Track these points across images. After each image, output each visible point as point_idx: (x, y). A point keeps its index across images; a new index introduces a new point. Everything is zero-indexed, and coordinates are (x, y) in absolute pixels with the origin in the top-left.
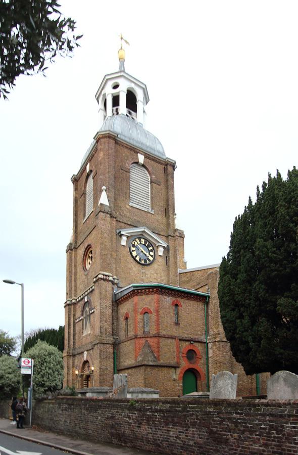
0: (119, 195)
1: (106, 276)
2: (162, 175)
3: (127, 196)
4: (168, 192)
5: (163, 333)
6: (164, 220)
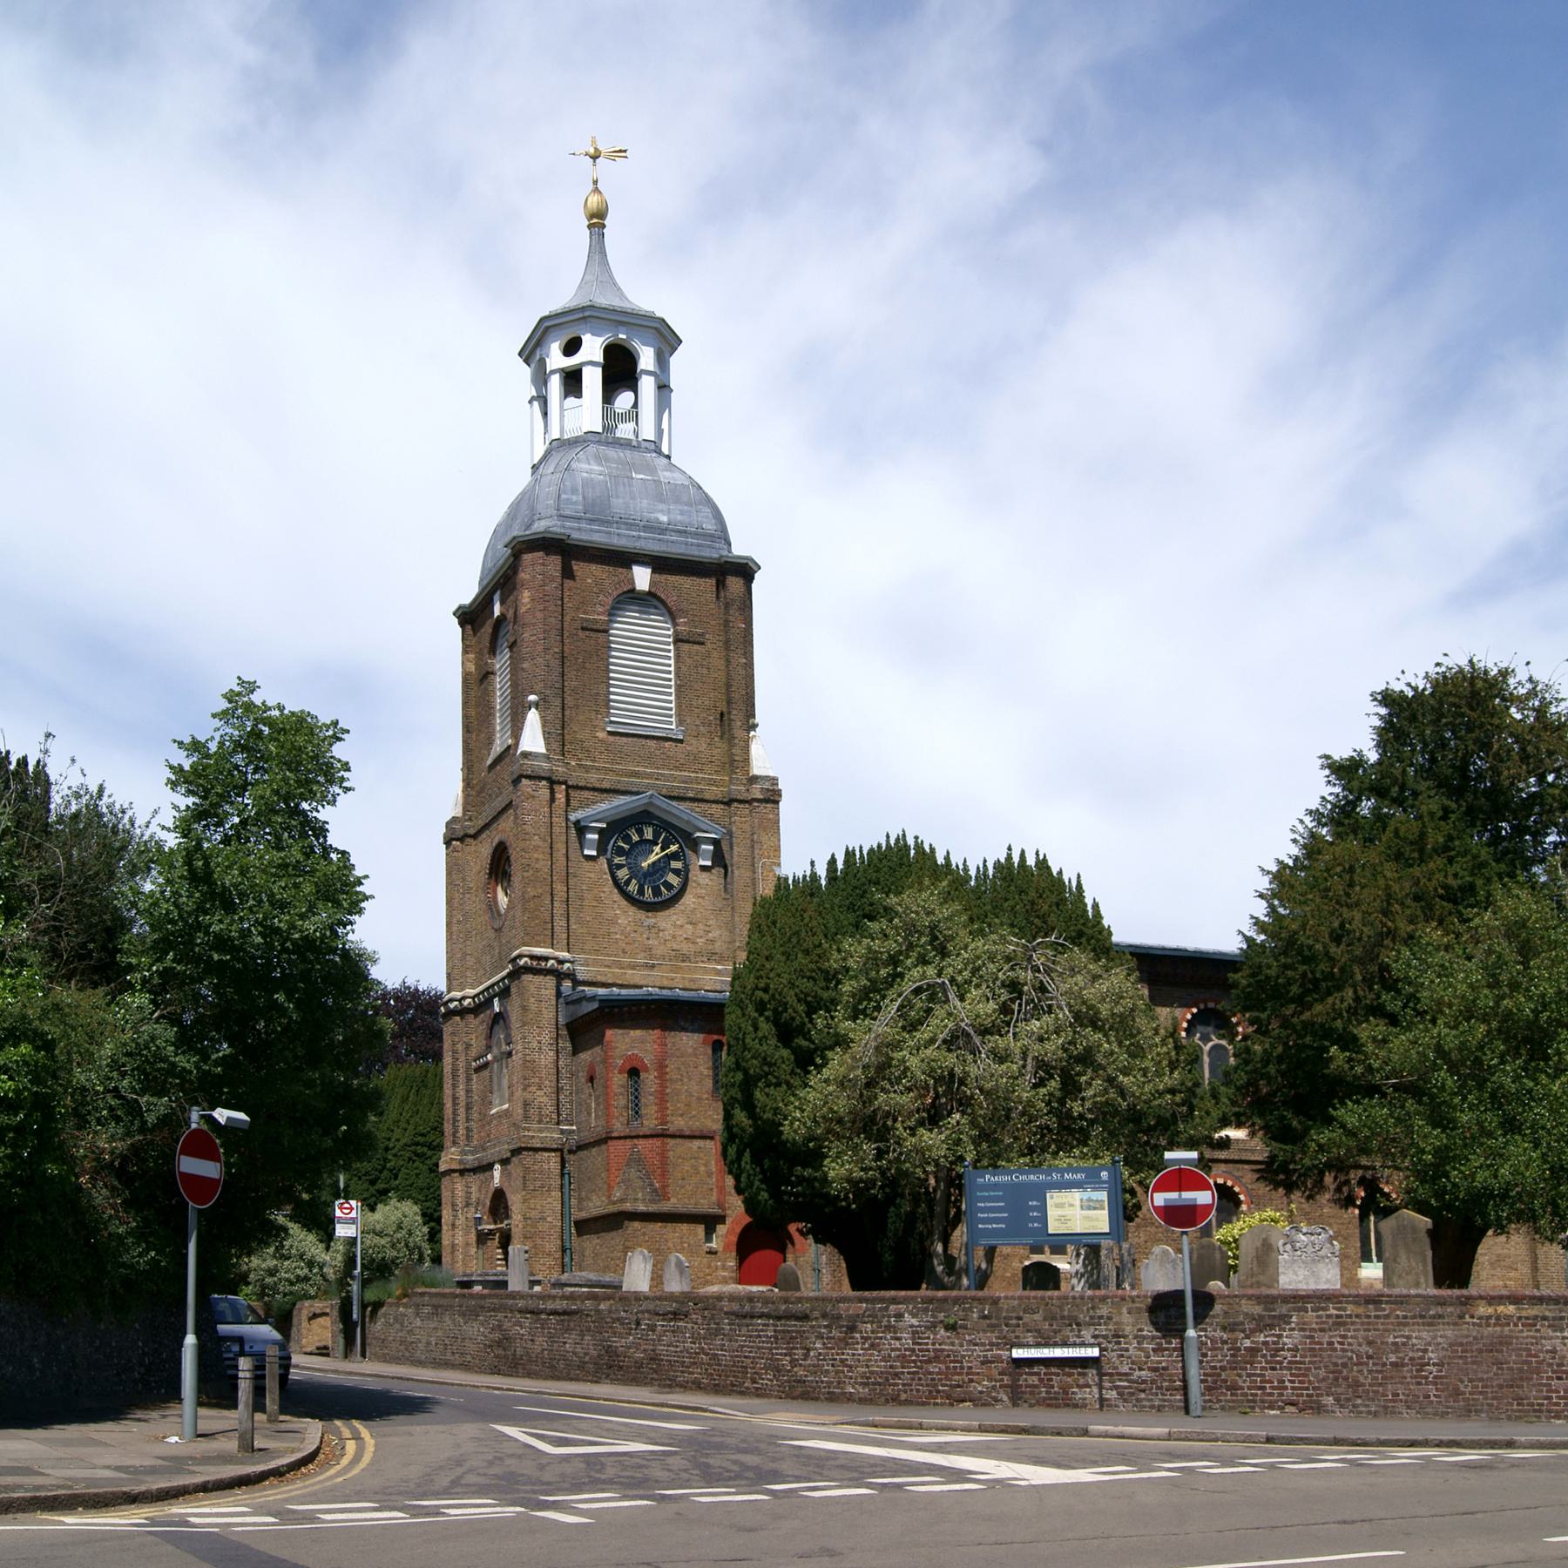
0: (577, 706)
2: (712, 606)
3: (604, 704)
5: (678, 1123)
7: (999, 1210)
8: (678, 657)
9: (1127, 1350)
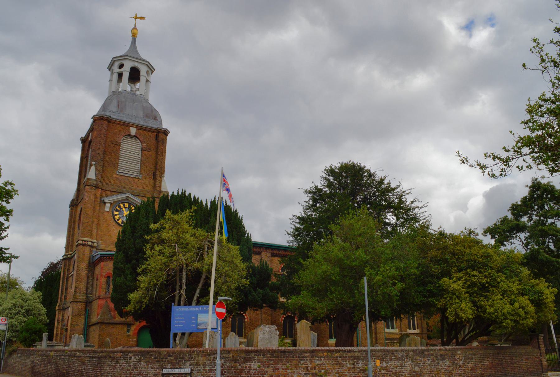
1: (85, 241)
3: (116, 165)
4: (157, 158)
6: (152, 183)
7: (182, 320)
8: (142, 155)
9: (200, 370)
